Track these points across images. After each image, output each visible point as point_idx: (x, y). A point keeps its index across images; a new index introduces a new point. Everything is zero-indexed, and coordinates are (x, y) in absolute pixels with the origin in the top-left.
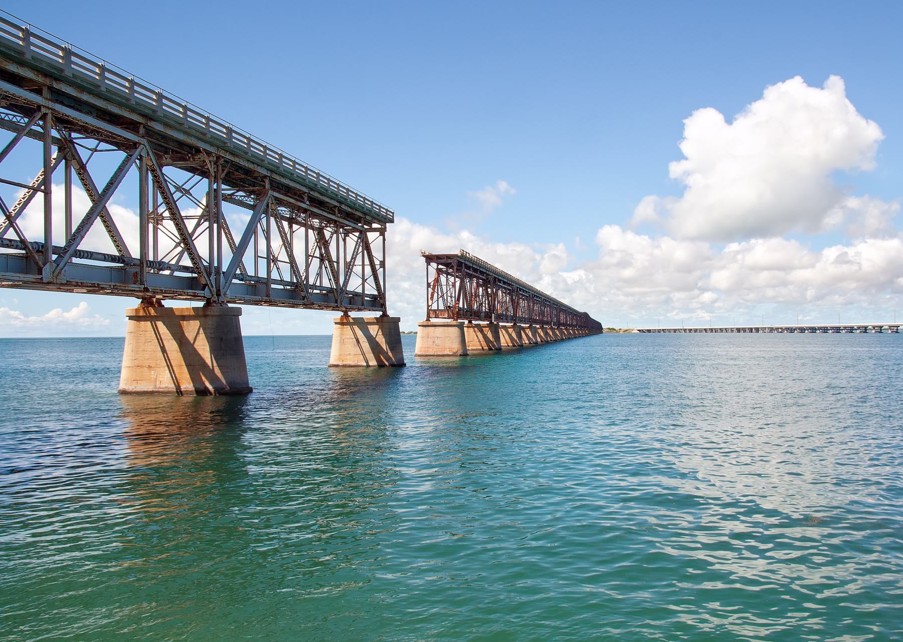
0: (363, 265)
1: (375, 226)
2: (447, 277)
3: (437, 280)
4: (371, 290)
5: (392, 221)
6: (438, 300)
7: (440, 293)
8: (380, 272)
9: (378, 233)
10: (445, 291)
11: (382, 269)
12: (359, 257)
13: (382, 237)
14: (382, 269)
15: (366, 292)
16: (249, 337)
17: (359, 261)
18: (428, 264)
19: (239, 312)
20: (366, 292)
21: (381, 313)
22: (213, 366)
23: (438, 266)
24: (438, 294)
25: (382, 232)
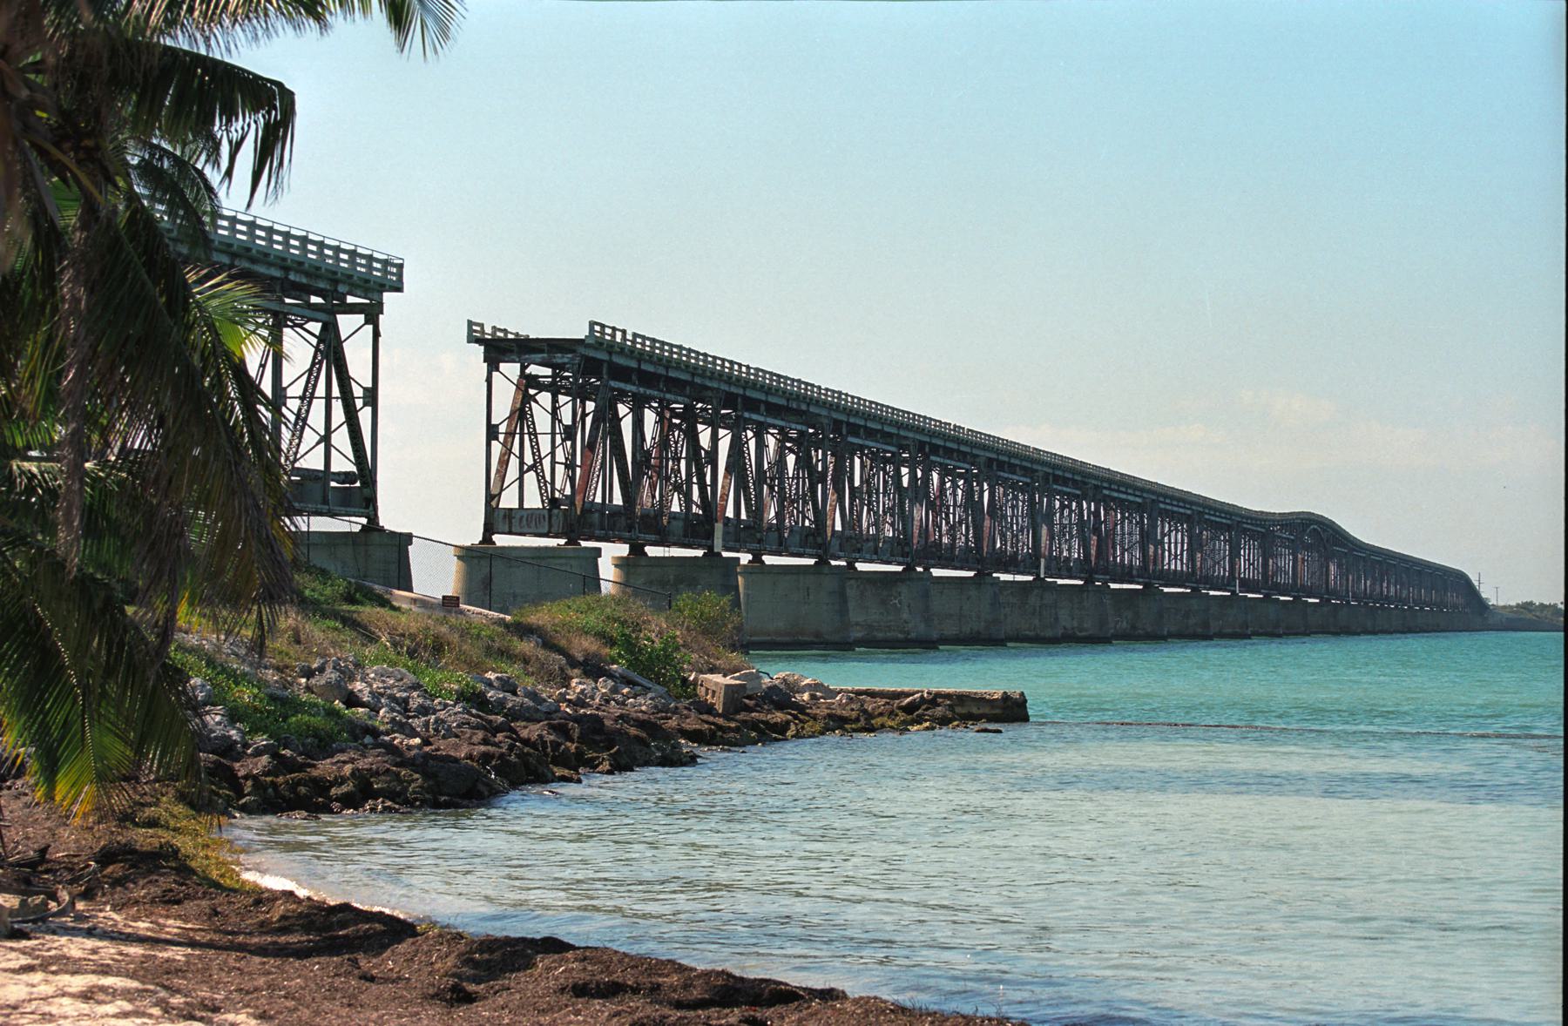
3: (521, 414)
4: (343, 463)
6: (521, 479)
7: (529, 460)
8: (365, 416)
9: (362, 317)
10: (545, 448)
11: (368, 409)
13: (370, 328)
18: (493, 363)
20: (334, 468)
23: (523, 368)
24: (522, 463)
25: (372, 314)
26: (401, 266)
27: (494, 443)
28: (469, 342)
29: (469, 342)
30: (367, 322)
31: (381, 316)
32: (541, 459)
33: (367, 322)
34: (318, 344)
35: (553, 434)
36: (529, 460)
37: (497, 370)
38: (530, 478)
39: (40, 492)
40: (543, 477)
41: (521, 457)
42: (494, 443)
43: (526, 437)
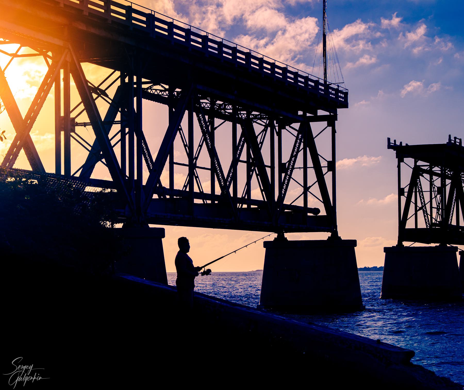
0: (305, 168)
1: (321, 113)
2: (431, 178)
3: (414, 183)
5: (345, 105)
6: (416, 214)
7: (419, 205)
8: (328, 178)
10: (427, 199)
11: (330, 173)
12: (301, 155)
13: (330, 129)
14: (330, 173)
15: (309, 206)
16: (168, 273)
17: (299, 162)
18: (400, 160)
19: (162, 233)
20: (309, 206)
21: (329, 234)
22: (201, 146)
23: (416, 162)
24: (416, 206)
26: (346, 94)
27: (402, 197)
28: (388, 148)
29: (388, 148)
30: (329, 125)
31: (336, 133)
32: (425, 205)
33: (329, 125)
34: (298, 135)
35: (431, 192)
36: (419, 205)
37: (403, 161)
38: (420, 213)
39: (69, 182)
40: (426, 212)
41: (416, 203)
42: (402, 197)
43: (418, 193)
